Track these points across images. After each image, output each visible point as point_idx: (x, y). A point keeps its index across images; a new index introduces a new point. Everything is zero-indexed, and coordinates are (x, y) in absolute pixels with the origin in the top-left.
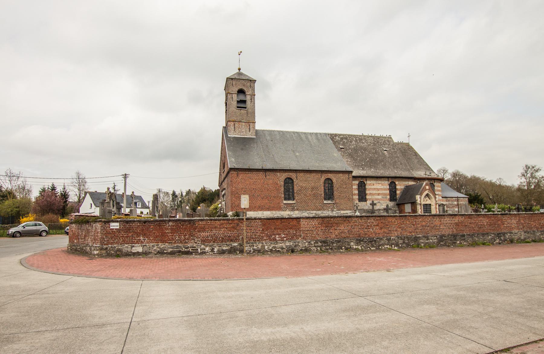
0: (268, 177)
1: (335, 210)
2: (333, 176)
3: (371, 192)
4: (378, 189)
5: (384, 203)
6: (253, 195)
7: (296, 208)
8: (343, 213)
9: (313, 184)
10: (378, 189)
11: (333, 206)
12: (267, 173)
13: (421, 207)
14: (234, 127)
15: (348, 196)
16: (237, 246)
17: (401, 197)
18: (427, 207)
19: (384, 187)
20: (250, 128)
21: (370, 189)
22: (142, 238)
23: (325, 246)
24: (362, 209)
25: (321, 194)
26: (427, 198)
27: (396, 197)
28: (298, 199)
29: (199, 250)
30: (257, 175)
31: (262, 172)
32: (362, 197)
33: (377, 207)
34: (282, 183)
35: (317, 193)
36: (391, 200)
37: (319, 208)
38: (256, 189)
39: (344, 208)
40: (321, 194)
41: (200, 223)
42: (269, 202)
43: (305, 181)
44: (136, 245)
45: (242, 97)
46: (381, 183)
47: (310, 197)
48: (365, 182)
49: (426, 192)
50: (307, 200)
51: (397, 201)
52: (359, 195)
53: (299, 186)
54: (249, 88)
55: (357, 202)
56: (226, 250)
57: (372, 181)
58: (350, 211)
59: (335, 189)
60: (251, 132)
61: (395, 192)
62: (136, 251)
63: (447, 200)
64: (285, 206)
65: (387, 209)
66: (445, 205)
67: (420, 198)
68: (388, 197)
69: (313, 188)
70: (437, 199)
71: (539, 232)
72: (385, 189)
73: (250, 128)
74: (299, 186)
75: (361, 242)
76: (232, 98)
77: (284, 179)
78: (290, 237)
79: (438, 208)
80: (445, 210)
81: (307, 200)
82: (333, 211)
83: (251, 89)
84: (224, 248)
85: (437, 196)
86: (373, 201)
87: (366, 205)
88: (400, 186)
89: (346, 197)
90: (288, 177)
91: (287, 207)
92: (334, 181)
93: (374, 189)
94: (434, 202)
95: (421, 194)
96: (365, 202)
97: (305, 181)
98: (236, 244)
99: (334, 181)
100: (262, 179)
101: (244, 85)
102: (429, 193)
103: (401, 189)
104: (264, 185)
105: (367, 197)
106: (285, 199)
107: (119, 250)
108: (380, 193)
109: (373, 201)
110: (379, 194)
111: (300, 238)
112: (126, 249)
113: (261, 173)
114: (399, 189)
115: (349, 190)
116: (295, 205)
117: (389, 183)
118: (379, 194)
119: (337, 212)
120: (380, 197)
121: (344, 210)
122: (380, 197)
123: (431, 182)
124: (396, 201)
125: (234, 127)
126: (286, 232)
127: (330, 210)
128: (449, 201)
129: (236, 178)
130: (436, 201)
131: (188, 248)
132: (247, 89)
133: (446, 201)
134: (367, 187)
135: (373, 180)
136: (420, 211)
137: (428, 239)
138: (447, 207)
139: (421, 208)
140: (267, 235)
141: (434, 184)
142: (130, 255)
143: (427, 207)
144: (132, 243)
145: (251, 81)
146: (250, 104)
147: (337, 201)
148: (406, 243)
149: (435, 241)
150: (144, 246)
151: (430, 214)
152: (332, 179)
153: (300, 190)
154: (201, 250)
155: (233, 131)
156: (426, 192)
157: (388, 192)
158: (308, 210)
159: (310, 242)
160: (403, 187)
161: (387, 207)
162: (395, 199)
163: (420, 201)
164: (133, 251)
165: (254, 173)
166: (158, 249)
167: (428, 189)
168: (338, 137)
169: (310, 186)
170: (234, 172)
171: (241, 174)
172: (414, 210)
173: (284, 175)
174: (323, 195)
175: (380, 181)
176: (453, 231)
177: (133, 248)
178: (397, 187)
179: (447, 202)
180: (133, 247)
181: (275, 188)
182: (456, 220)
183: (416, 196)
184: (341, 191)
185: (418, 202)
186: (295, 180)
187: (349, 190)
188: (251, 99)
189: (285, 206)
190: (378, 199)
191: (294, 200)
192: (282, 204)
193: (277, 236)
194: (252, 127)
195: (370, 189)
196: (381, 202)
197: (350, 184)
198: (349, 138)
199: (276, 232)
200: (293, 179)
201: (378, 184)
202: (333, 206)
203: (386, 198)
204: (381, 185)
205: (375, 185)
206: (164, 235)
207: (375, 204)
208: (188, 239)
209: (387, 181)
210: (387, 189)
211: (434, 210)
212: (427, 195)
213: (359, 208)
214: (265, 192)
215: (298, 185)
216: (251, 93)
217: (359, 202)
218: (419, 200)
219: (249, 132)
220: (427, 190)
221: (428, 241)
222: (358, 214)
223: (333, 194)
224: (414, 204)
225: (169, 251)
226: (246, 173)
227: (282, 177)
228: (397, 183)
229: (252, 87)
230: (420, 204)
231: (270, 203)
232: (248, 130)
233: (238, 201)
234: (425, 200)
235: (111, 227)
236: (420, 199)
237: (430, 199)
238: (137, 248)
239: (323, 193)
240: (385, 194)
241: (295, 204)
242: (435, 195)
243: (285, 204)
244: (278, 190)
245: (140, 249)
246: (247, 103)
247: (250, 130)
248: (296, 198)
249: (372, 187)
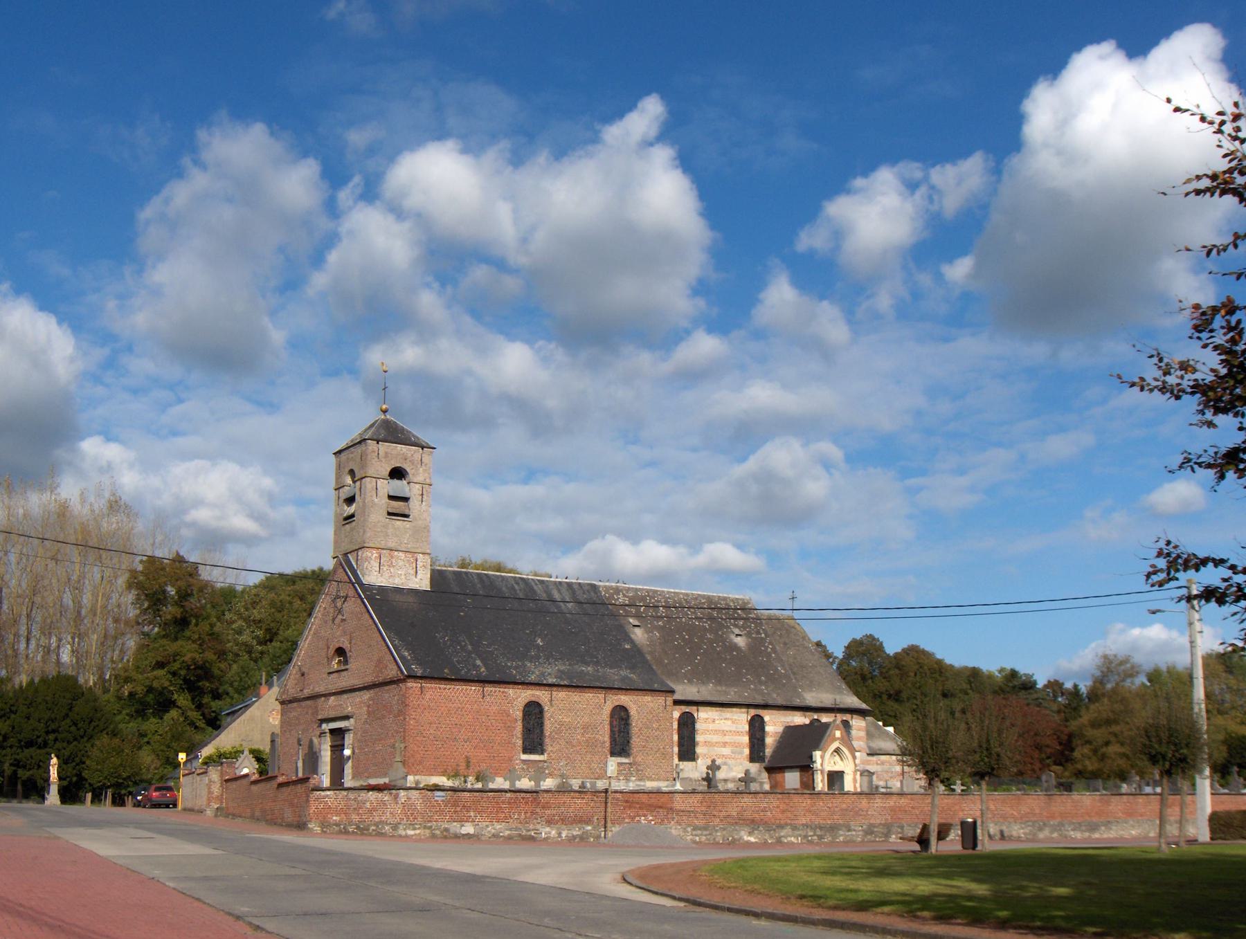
0: (488, 699)
1: (634, 778)
2: (631, 701)
3: (709, 737)
4: (724, 733)
5: (735, 766)
6: (455, 738)
7: (547, 772)
8: (650, 785)
9: (586, 719)
10: (723, 731)
11: (629, 770)
12: (485, 689)
13: (823, 778)
14: (380, 563)
15: (663, 748)
16: (590, 830)
17: (774, 752)
18: (835, 778)
19: (736, 728)
20: (416, 567)
21: (706, 731)
22: (472, 814)
23: (706, 835)
24: (686, 778)
25: (604, 742)
26: (837, 758)
27: (764, 753)
28: (551, 751)
29: (543, 834)
30: (464, 694)
31: (476, 686)
32: (687, 751)
33: (720, 775)
34: (519, 714)
35: (594, 738)
36: (752, 759)
37: (597, 773)
38: (461, 725)
39: (653, 776)
40: (604, 742)
41: (545, 795)
42: (490, 756)
43: (569, 710)
44: (466, 824)
45: (398, 486)
46: (731, 719)
47: (578, 748)
48: (696, 715)
49: (836, 745)
50: (571, 754)
51: (766, 761)
52: (680, 745)
53: (556, 721)
54: (419, 466)
55: (676, 760)
56: (577, 835)
57: (710, 713)
58: (666, 783)
59: (634, 730)
60: (419, 577)
61: (763, 740)
62: (466, 832)
63: (879, 762)
64: (525, 767)
65: (747, 779)
66: (873, 773)
67: (822, 757)
68: (747, 751)
69: (585, 728)
70: (857, 761)
71: (82, 581)
72: (738, 733)
73: (416, 567)
74: (556, 721)
75: (756, 832)
76: (377, 489)
77: (524, 704)
78: (660, 821)
79: (858, 781)
80: (874, 786)
81: (571, 754)
82: (628, 780)
83: (421, 469)
84: (575, 833)
85: (857, 754)
86: (713, 761)
87: (694, 771)
88: (775, 724)
89: (659, 749)
90: (533, 699)
91: (528, 769)
92: (632, 713)
93: (716, 732)
94: (852, 766)
95: (824, 750)
96: (694, 763)
97: (569, 710)
98: (589, 828)
99: (633, 712)
100: (476, 702)
101: (406, 459)
102: (841, 747)
103: (776, 733)
104: (479, 717)
105: (699, 750)
106: (525, 751)
107: (446, 830)
108: (728, 741)
109: (713, 761)
110: (725, 744)
111: (672, 822)
112: (454, 829)
113: (473, 688)
114: (770, 734)
115: (665, 733)
116: (545, 764)
117: (749, 718)
118: (725, 744)
119: (638, 783)
120: (726, 751)
121: (653, 780)
122: (726, 751)
123: (844, 719)
124: (764, 761)
125: (380, 563)
126: (654, 813)
127: (621, 778)
128: (883, 765)
129: (419, 698)
130: (856, 765)
131: (529, 831)
132: (412, 469)
133: (877, 764)
134: (698, 726)
135: (712, 711)
136: (820, 783)
137: (849, 830)
138: (877, 777)
139: (822, 781)
140: (630, 816)
141: (851, 722)
142: (459, 837)
143: (835, 778)
144: (462, 821)
145: (423, 449)
146: (418, 506)
147: (639, 759)
148: (818, 836)
149: (860, 833)
150: (476, 825)
151: (813, 792)
152: (628, 708)
153: (559, 732)
154: (545, 834)
155: (376, 573)
156: (836, 745)
157: (746, 739)
158: (575, 778)
159: (685, 829)
160: (780, 729)
161: (745, 774)
162: (761, 757)
163: (822, 765)
164: (463, 832)
165: (458, 687)
166: (493, 831)
167: (838, 738)
168: (624, 596)
169: (579, 722)
170: (415, 685)
171: (429, 689)
172: (808, 785)
173: (523, 695)
174: (608, 744)
175: (728, 714)
176: (887, 819)
177: (463, 828)
178: (768, 729)
179: (879, 766)
180: (463, 826)
181: (502, 725)
182: (891, 802)
183: (814, 753)
184: (648, 737)
185: (818, 765)
186: (546, 708)
187: (665, 733)
188: (422, 495)
189: (525, 767)
190: (723, 755)
191: (542, 754)
192: (518, 762)
193: (643, 818)
194: (421, 564)
195: (706, 731)
196: (729, 762)
197: (667, 719)
198: (650, 600)
199: (641, 813)
200: (542, 704)
201: (725, 719)
202: (629, 770)
203: (741, 753)
204: (729, 722)
205: (717, 722)
206: (500, 810)
207: (719, 768)
208: (529, 818)
209: (744, 713)
210: (745, 733)
211: (850, 783)
212: (837, 751)
213: (682, 775)
214: (481, 732)
215: (554, 718)
216: (423, 479)
217: (679, 761)
218: (819, 761)
219: (414, 577)
220: (836, 739)
221: (850, 833)
222: (678, 787)
223: (628, 742)
224: (806, 768)
225: (506, 834)
226: (440, 688)
227: (519, 699)
228: (767, 718)
229: (426, 465)
230: (822, 772)
231: (492, 758)
232: (413, 572)
233: (422, 750)
234: (832, 762)
235: (436, 798)
236: (822, 761)
237: (842, 760)
238: (467, 828)
239: (607, 738)
240: (738, 745)
241: (545, 762)
242: (853, 751)
243: (524, 761)
244: (510, 729)
245: (469, 829)
246: (411, 502)
247: (416, 572)
248: (549, 748)
249: (711, 726)
